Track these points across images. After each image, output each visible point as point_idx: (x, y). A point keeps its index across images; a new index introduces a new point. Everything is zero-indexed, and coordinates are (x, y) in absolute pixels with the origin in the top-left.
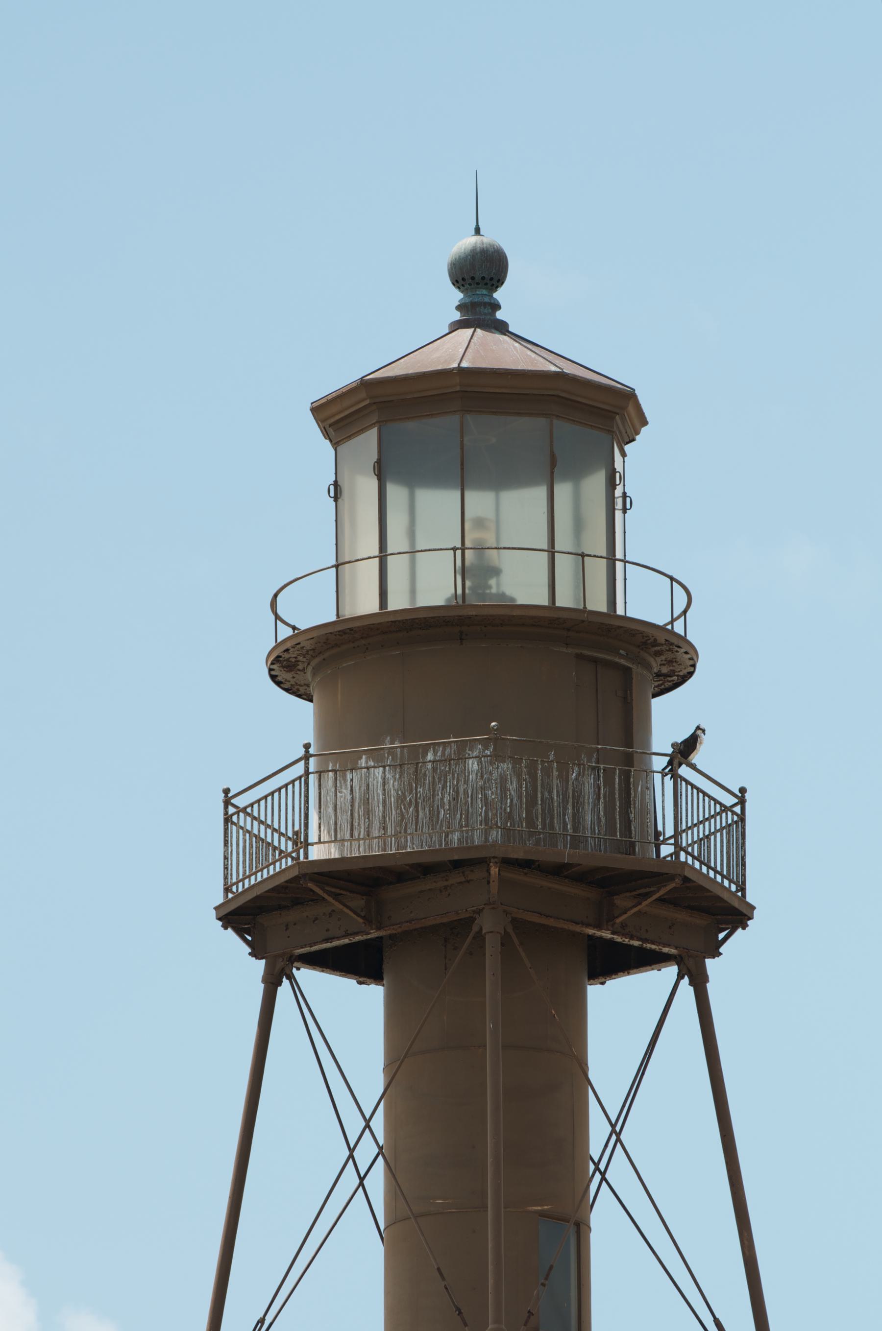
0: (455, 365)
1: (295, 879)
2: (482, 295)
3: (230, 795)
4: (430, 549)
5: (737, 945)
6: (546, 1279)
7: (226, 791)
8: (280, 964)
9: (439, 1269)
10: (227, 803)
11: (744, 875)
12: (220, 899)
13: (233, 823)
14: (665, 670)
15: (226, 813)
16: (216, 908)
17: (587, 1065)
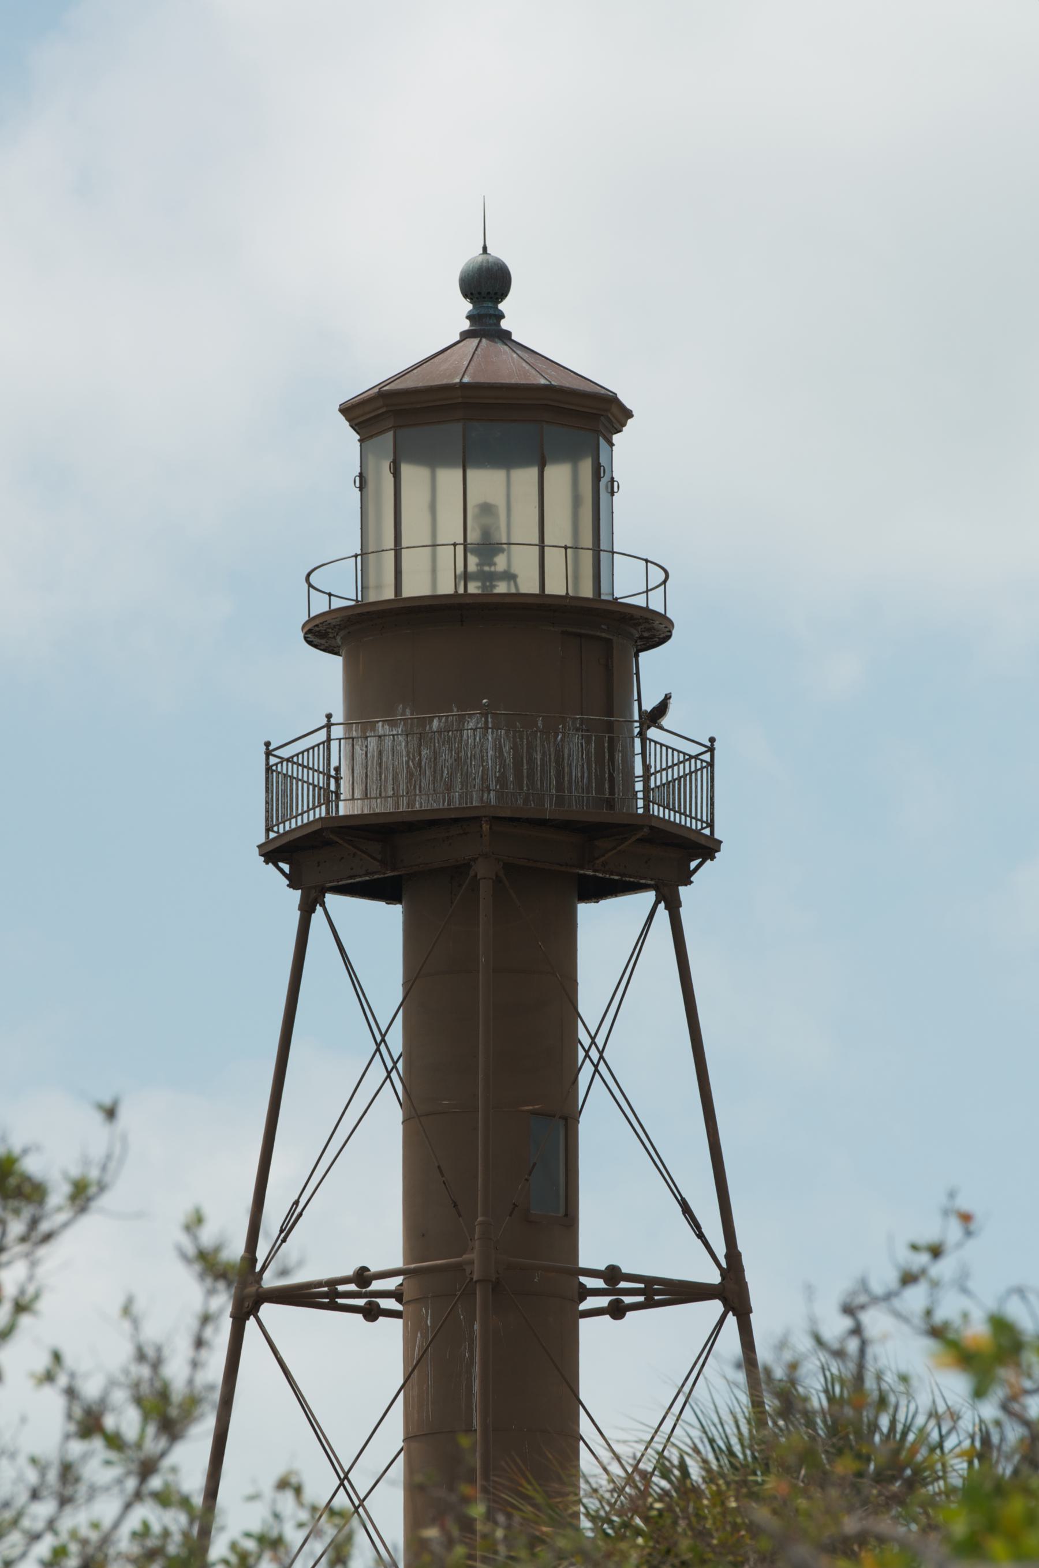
0: (457, 380)
1: (321, 830)
2: (488, 307)
3: (271, 748)
4: (454, 521)
6: (530, 1175)
7: (267, 744)
8: (313, 894)
9: (439, 1167)
10: (268, 754)
11: (712, 814)
13: (273, 771)
14: (646, 634)
15: (267, 763)
16: (259, 847)
17: (576, 981)
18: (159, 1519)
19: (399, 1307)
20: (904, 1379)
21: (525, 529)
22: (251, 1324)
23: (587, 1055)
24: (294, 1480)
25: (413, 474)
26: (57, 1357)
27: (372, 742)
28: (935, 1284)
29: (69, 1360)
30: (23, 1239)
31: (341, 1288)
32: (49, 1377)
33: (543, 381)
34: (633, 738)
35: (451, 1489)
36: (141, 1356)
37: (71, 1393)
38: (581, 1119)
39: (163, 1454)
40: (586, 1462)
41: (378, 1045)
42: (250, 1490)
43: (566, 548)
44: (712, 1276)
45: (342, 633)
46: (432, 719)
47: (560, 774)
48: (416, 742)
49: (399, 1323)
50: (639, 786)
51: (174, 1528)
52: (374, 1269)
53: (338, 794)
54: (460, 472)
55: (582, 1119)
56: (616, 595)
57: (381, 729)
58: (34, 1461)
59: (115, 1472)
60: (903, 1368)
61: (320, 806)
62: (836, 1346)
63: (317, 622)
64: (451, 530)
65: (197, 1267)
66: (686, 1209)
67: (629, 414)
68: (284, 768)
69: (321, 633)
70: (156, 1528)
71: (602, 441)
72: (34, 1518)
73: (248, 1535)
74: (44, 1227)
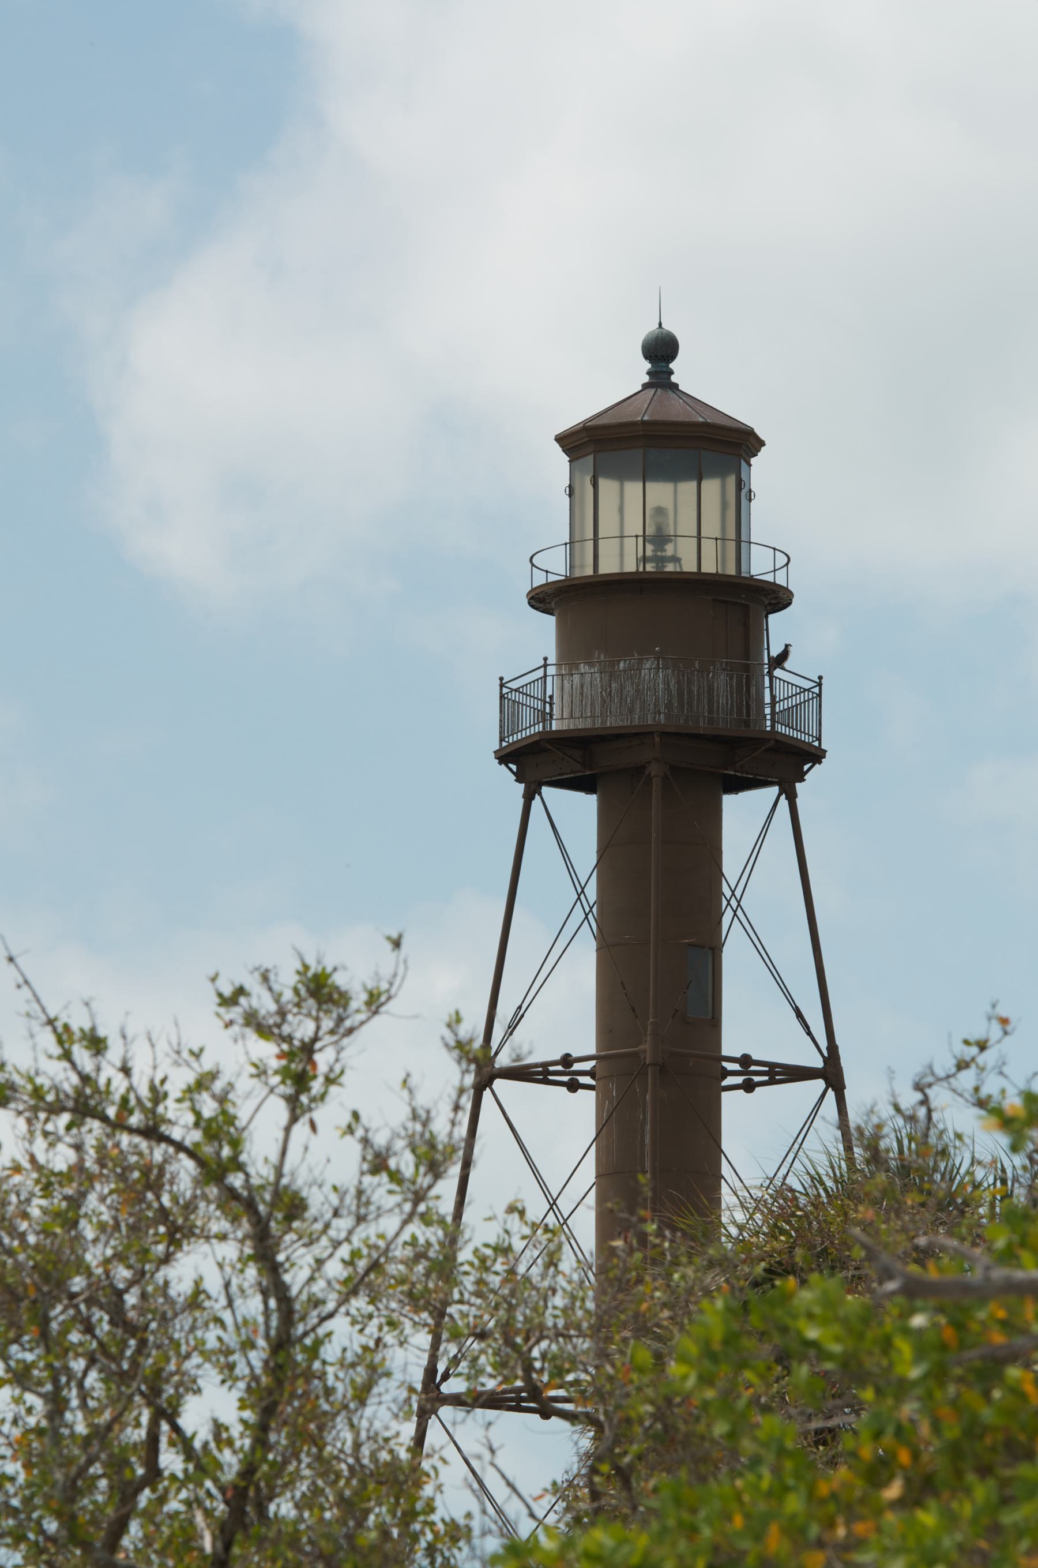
4: (642, 520)
5: (815, 774)
7: (501, 679)
8: (533, 787)
10: (502, 686)
11: (820, 731)
12: (497, 747)
14: (773, 602)
15: (501, 692)
18: (424, 1234)
19: (593, 1082)
20: (959, 1136)
21: (687, 525)
22: (487, 1094)
23: (729, 904)
24: (519, 1206)
25: (608, 487)
26: (356, 1115)
27: (576, 678)
28: (982, 1069)
29: (364, 1119)
30: (332, 1032)
31: (551, 1068)
32: (350, 1130)
33: (701, 420)
34: (764, 676)
35: (632, 1212)
36: (415, 1116)
37: (365, 1141)
38: (724, 949)
39: (430, 1187)
40: (727, 1197)
41: (579, 895)
42: (490, 1214)
43: (716, 539)
44: (817, 1062)
45: (555, 600)
46: (619, 662)
47: (710, 702)
48: (607, 678)
49: (593, 1093)
50: (768, 711)
51: (433, 1240)
52: (575, 1055)
53: (551, 715)
54: (641, 484)
55: (726, 949)
56: (752, 573)
57: (583, 668)
58: (335, 1188)
59: (398, 1198)
60: (959, 1130)
61: (538, 723)
62: (908, 1113)
63: (537, 591)
64: (634, 525)
65: (456, 1053)
66: (799, 1015)
67: (762, 443)
68: (513, 696)
69: (541, 599)
70: (422, 1241)
71: (743, 463)
72: (338, 1230)
73: (487, 1245)
74: (348, 1023)
